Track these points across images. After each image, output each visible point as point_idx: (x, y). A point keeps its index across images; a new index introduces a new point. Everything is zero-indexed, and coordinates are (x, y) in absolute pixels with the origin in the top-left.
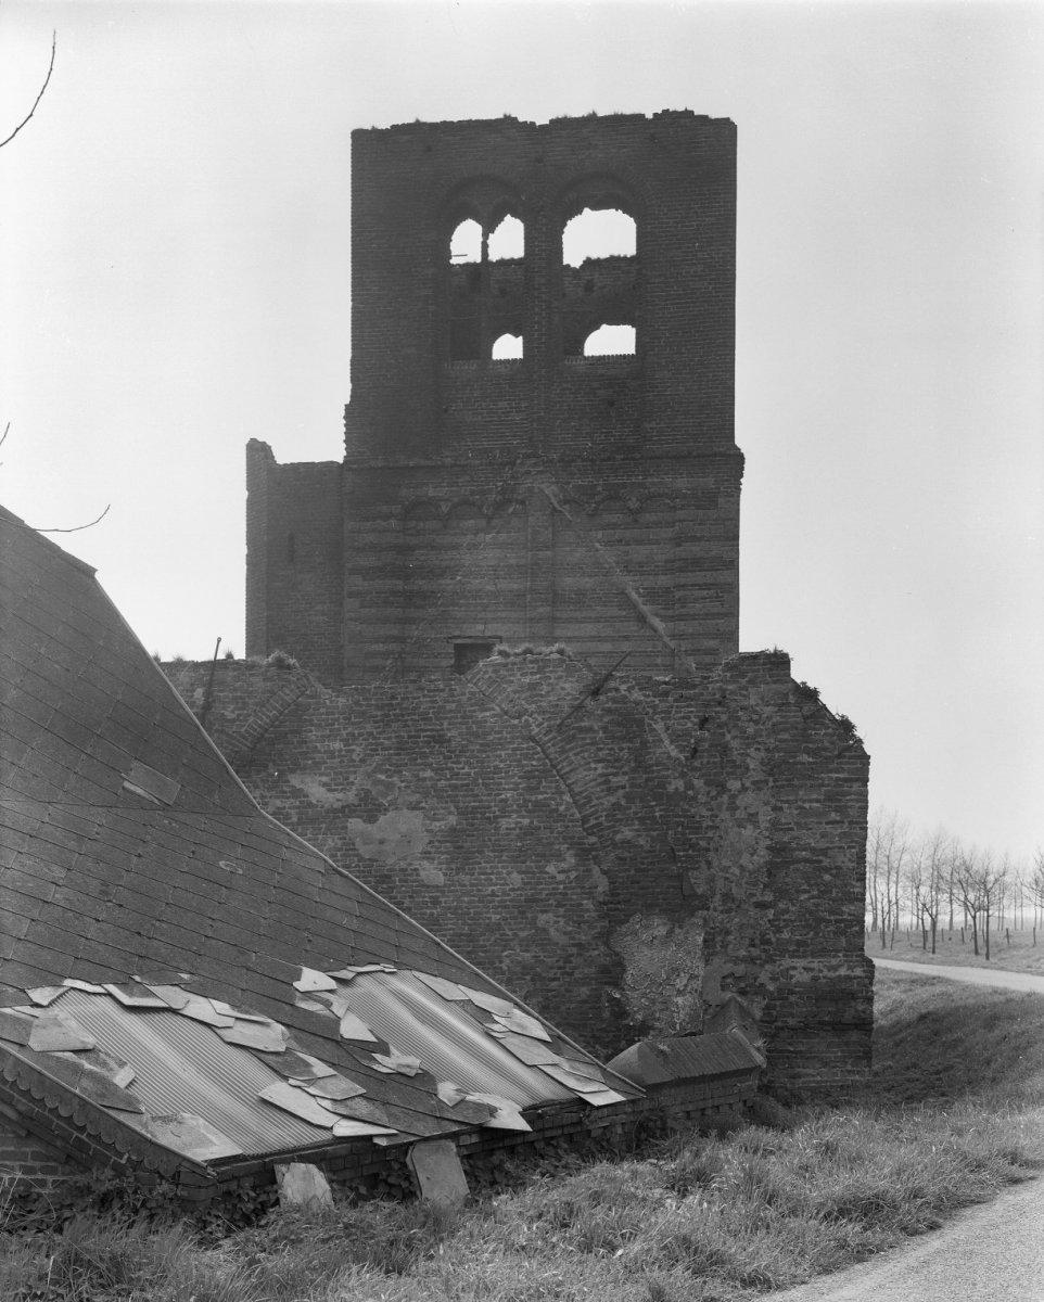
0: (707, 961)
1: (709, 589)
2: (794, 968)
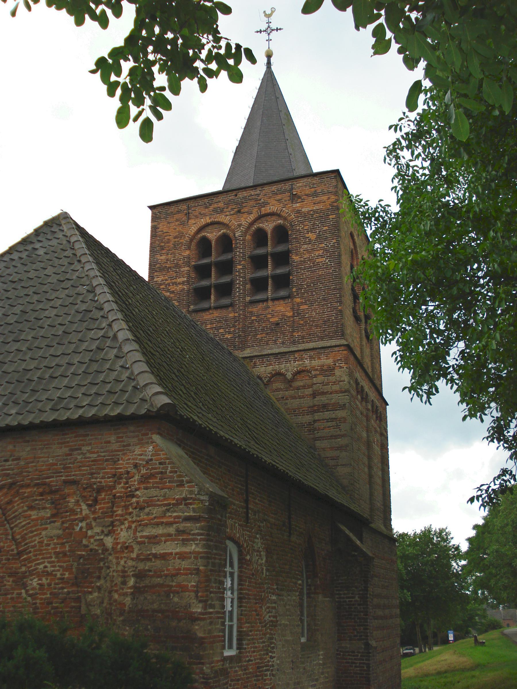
1: (333, 421)
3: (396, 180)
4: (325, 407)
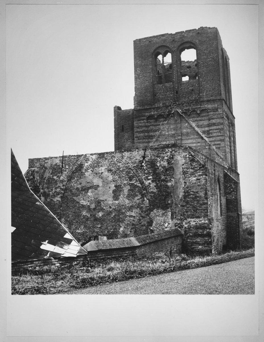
0: (172, 220)
2: (191, 221)
3: (94, 157)
4: (214, 124)
